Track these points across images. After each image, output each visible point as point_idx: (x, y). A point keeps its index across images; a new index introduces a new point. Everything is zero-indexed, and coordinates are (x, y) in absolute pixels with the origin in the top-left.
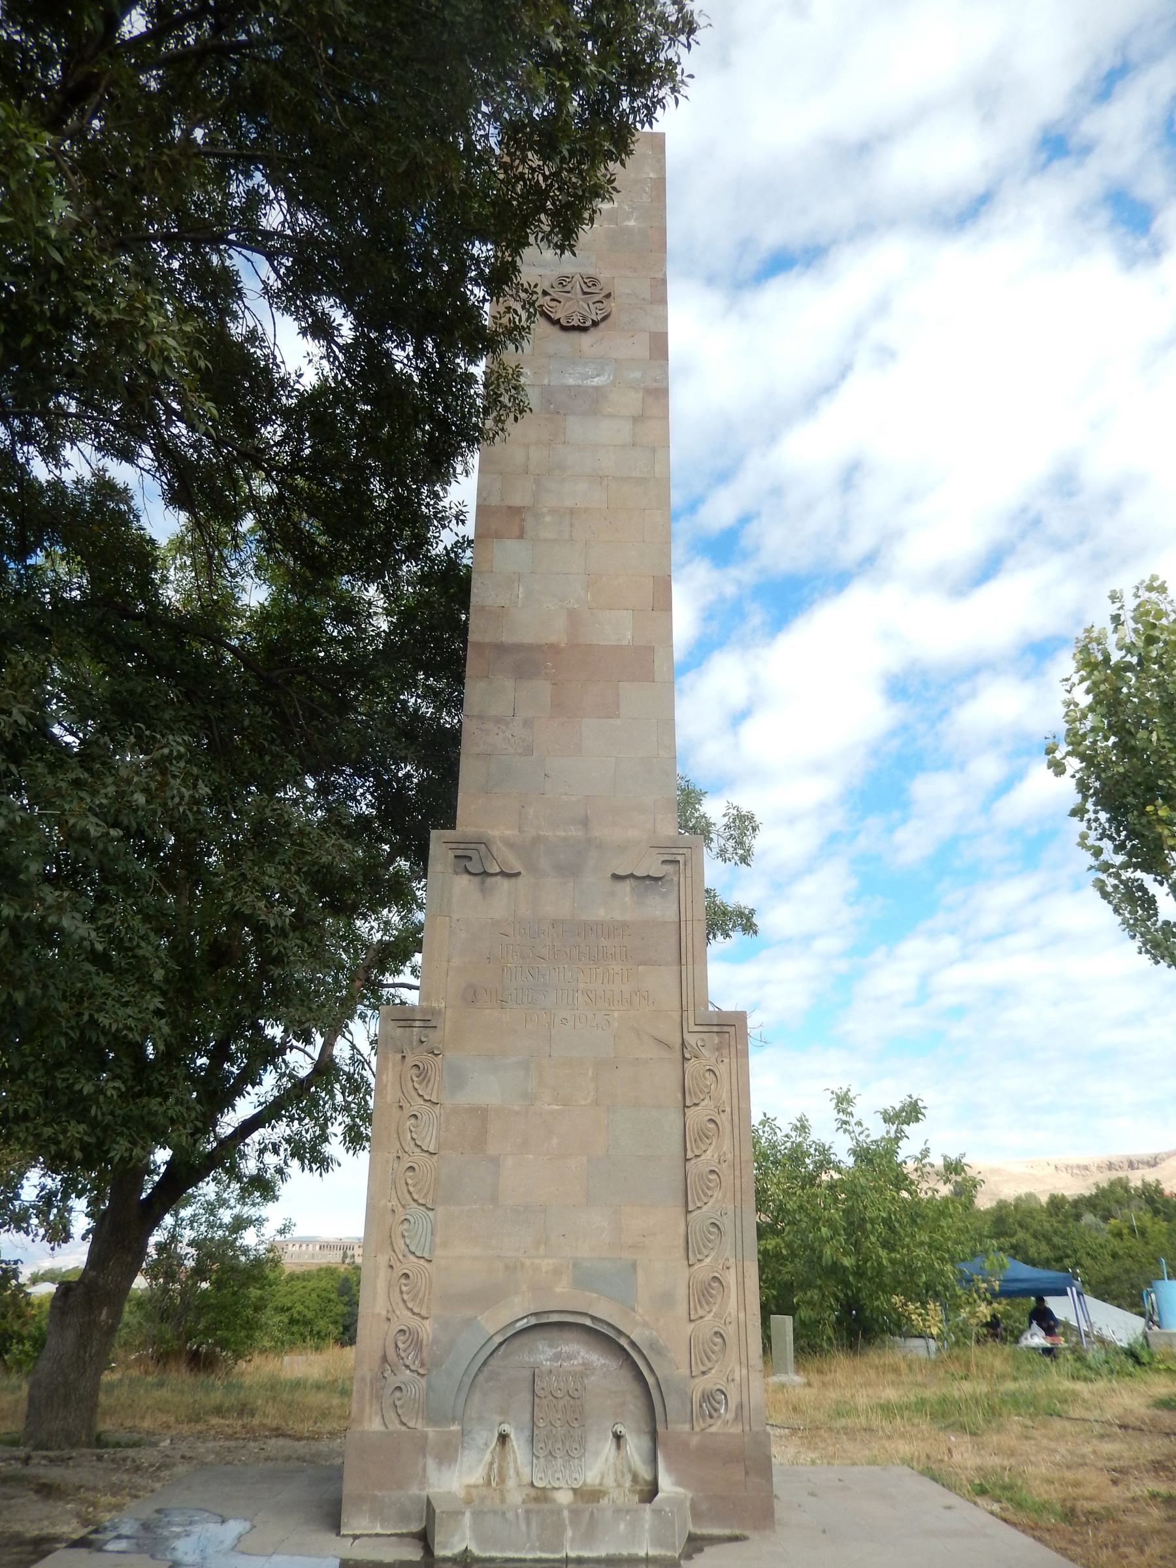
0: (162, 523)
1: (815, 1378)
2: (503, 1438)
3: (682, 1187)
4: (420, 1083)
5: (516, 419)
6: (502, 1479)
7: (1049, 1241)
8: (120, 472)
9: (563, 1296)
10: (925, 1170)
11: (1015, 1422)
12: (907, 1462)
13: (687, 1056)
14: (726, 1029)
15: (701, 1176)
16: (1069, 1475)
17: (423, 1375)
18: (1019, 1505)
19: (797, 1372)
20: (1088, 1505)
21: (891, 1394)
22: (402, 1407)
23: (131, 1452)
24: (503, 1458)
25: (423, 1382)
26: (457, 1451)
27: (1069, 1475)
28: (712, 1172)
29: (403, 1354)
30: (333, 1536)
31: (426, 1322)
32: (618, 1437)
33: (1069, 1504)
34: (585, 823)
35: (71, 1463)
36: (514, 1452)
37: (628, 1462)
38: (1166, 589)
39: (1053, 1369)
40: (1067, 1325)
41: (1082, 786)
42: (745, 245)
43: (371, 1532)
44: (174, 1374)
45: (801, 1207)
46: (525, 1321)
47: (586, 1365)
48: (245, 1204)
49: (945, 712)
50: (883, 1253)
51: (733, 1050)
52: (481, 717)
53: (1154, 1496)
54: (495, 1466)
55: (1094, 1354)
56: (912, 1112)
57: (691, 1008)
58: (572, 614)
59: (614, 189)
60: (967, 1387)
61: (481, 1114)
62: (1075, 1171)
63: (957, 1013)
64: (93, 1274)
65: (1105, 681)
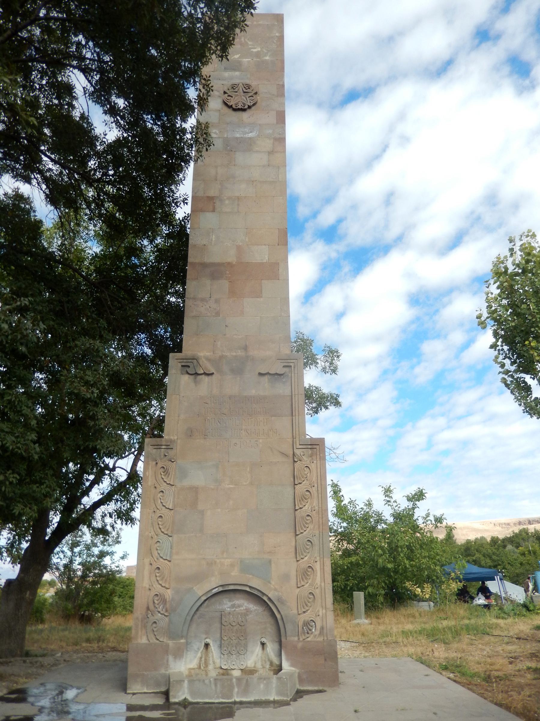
0: (44, 212)
1: (374, 620)
2: (207, 645)
3: (293, 523)
4: (165, 476)
5: (207, 150)
6: (206, 664)
7: (490, 558)
8: (25, 189)
9: (235, 577)
10: (428, 523)
11: (466, 638)
12: (410, 656)
13: (296, 460)
14: (314, 447)
15: (302, 518)
16: (489, 660)
17: (167, 616)
18: (463, 674)
19: (366, 618)
20: (496, 674)
21: (409, 627)
22: (156, 631)
23: (40, 659)
24: (207, 655)
25: (167, 619)
26: (183, 652)
27: (489, 660)
28: (308, 515)
29: (157, 606)
30: (123, 694)
31: (168, 591)
32: (263, 644)
33: (487, 673)
34: (245, 348)
35: (10, 664)
36: (212, 652)
37: (268, 655)
38: (536, 236)
39: (488, 614)
40: (496, 595)
41: (496, 334)
42: (335, 87)
43: (141, 692)
44: (73, 625)
45: (368, 541)
46: (217, 589)
47: (247, 610)
48: (104, 545)
49: (437, 311)
50: (407, 562)
51: (318, 457)
52: (194, 299)
53: (529, 668)
54: (203, 659)
55: (507, 607)
56: (420, 496)
57: (298, 437)
58: (239, 248)
59: (246, 25)
60: (445, 623)
61: (195, 490)
62: (503, 526)
63: (446, 453)
64: (22, 575)
65: (506, 282)
